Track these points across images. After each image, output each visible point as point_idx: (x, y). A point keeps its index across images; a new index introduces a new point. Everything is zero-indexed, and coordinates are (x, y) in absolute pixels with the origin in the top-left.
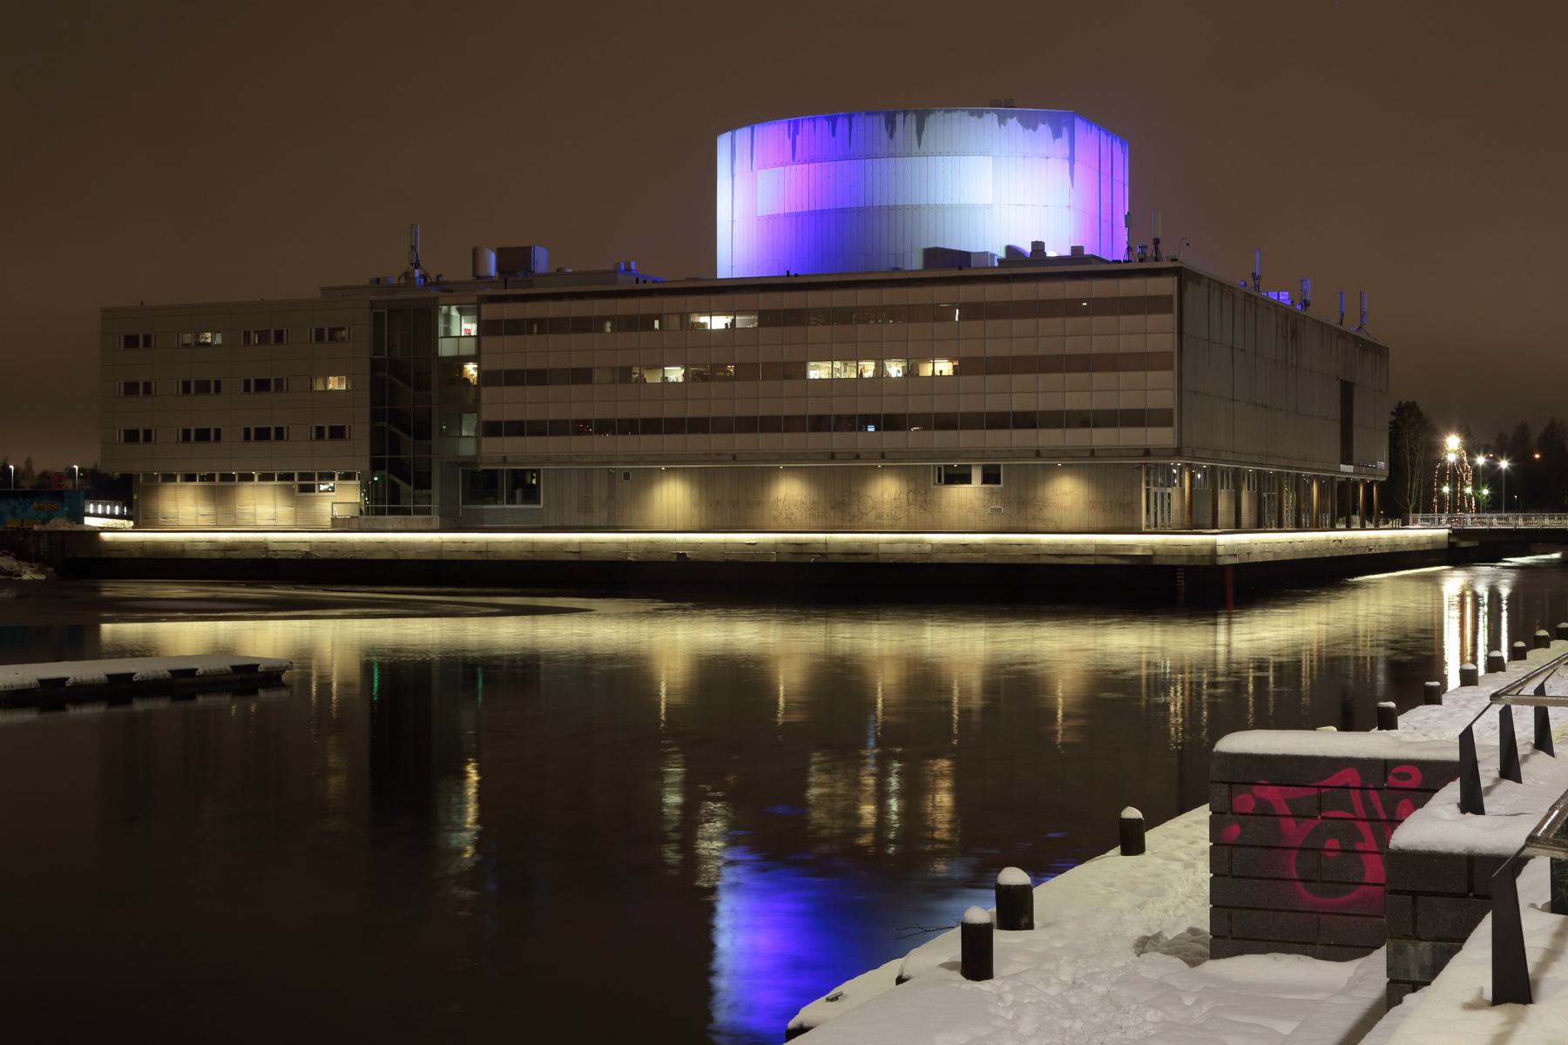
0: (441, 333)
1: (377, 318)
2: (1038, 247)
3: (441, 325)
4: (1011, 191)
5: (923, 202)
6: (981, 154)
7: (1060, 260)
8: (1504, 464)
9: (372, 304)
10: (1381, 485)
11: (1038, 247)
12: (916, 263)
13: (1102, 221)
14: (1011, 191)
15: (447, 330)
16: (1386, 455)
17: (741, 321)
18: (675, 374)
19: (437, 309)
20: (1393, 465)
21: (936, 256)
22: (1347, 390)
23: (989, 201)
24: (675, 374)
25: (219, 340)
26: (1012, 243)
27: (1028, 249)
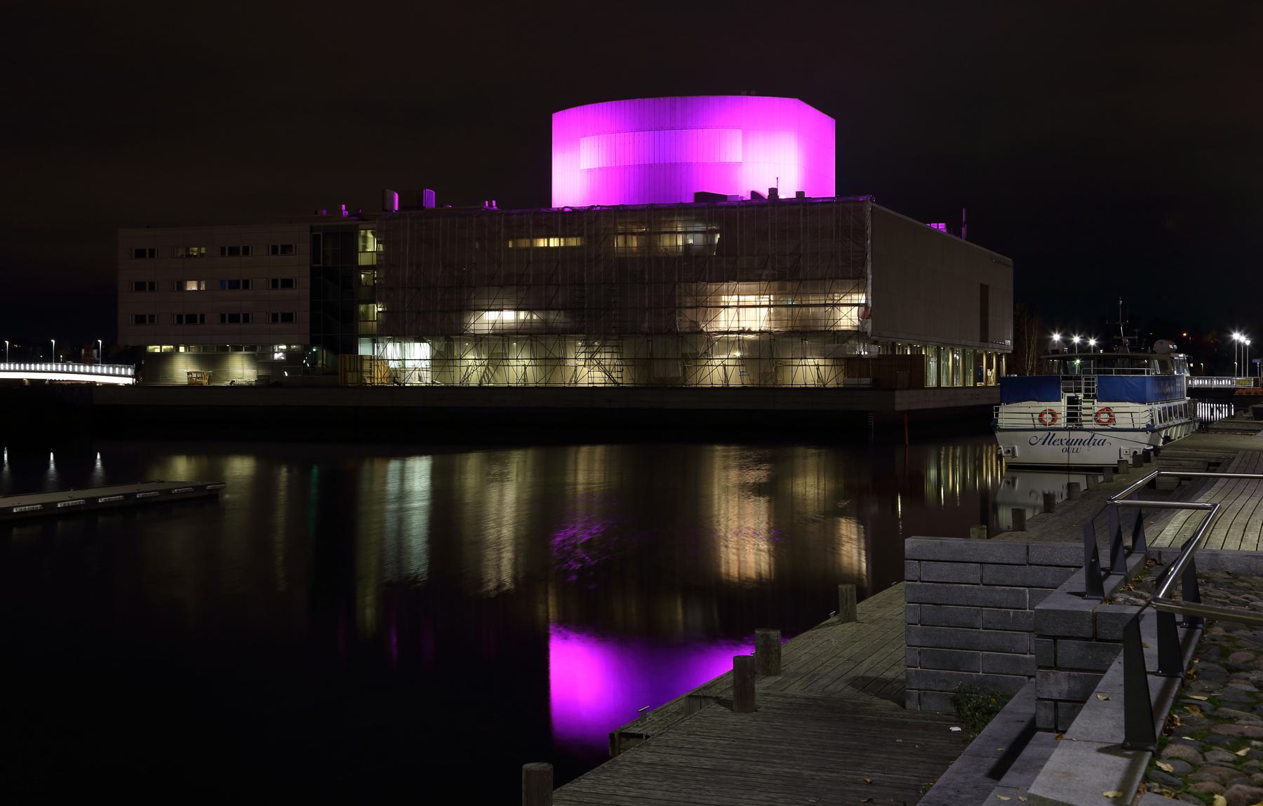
0: (361, 249)
1: (315, 240)
2: (773, 192)
3: (361, 244)
4: (773, 156)
5: (694, 161)
6: (734, 127)
7: (789, 201)
8: (1092, 342)
9: (312, 229)
10: (1008, 355)
11: (773, 192)
12: (690, 200)
13: (811, 171)
14: (773, 156)
15: (365, 247)
16: (1011, 336)
17: (573, 242)
18: (192, 286)
19: (357, 233)
20: (1016, 341)
21: (703, 197)
22: (984, 289)
23: (739, 159)
24: (192, 286)
25: (203, 250)
26: (756, 190)
27: (766, 193)
